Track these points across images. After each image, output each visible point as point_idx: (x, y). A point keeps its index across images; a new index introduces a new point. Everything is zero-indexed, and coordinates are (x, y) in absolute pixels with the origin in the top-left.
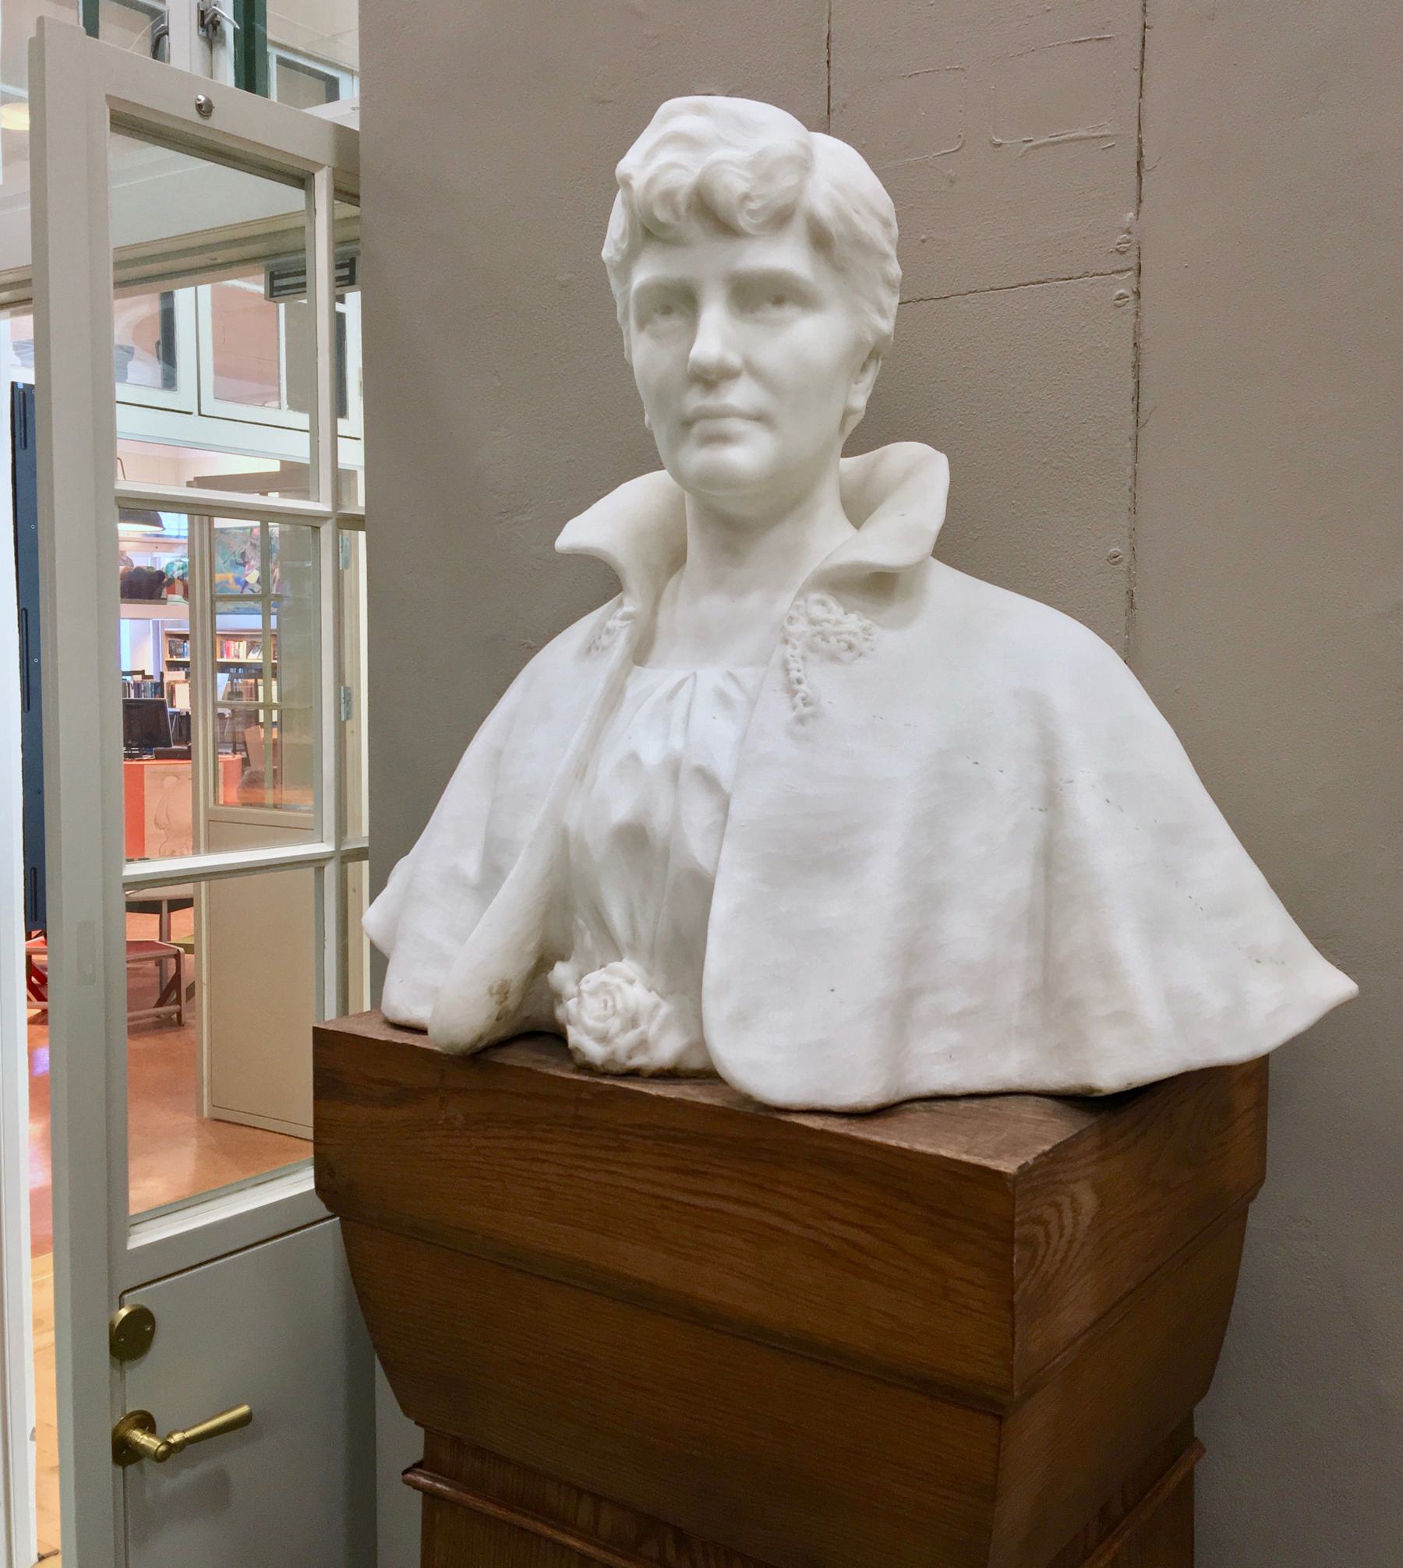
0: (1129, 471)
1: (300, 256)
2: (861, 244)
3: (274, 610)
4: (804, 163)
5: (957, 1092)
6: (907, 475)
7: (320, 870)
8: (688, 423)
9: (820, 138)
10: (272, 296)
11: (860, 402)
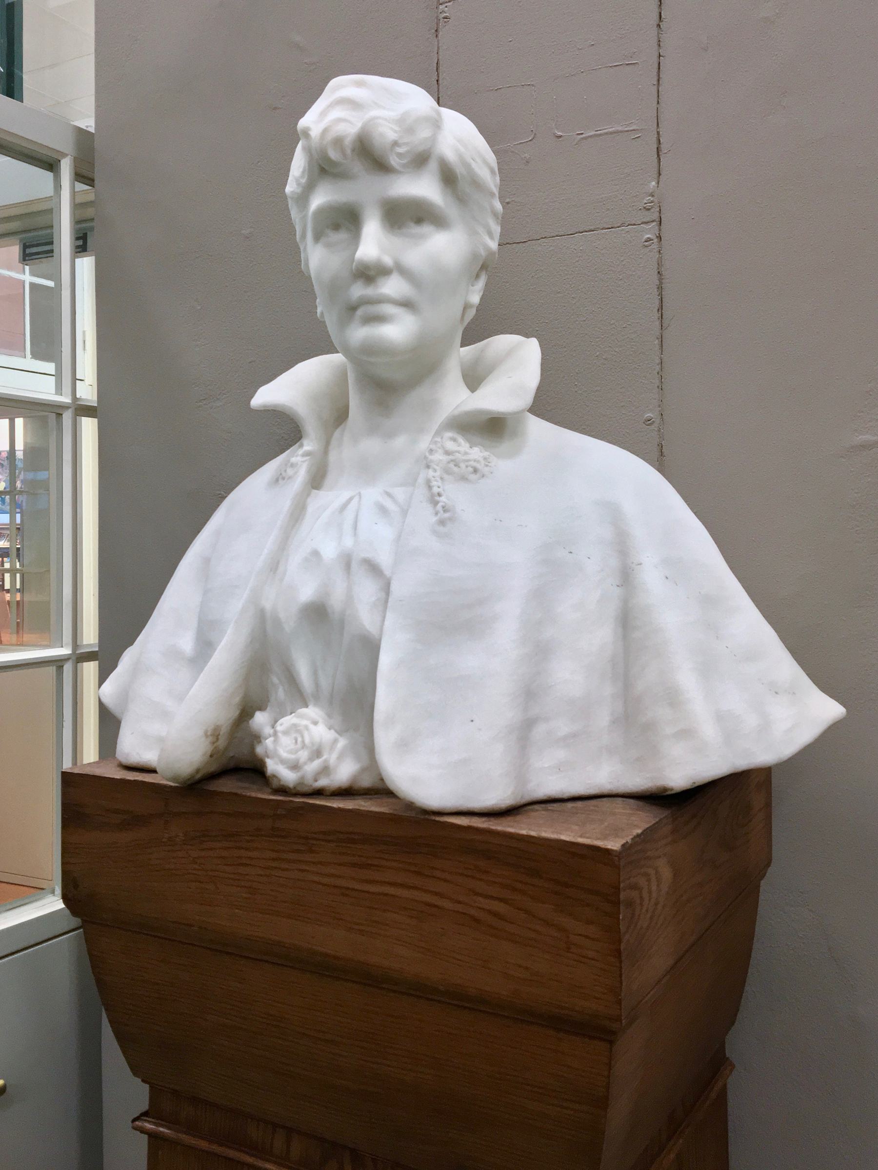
0: (658, 361)
1: (49, 231)
2: (476, 183)
3: (18, 510)
4: (437, 124)
6: (510, 353)
7: (60, 668)
8: (353, 308)
9: (446, 112)
10: (24, 260)
11: (475, 299)
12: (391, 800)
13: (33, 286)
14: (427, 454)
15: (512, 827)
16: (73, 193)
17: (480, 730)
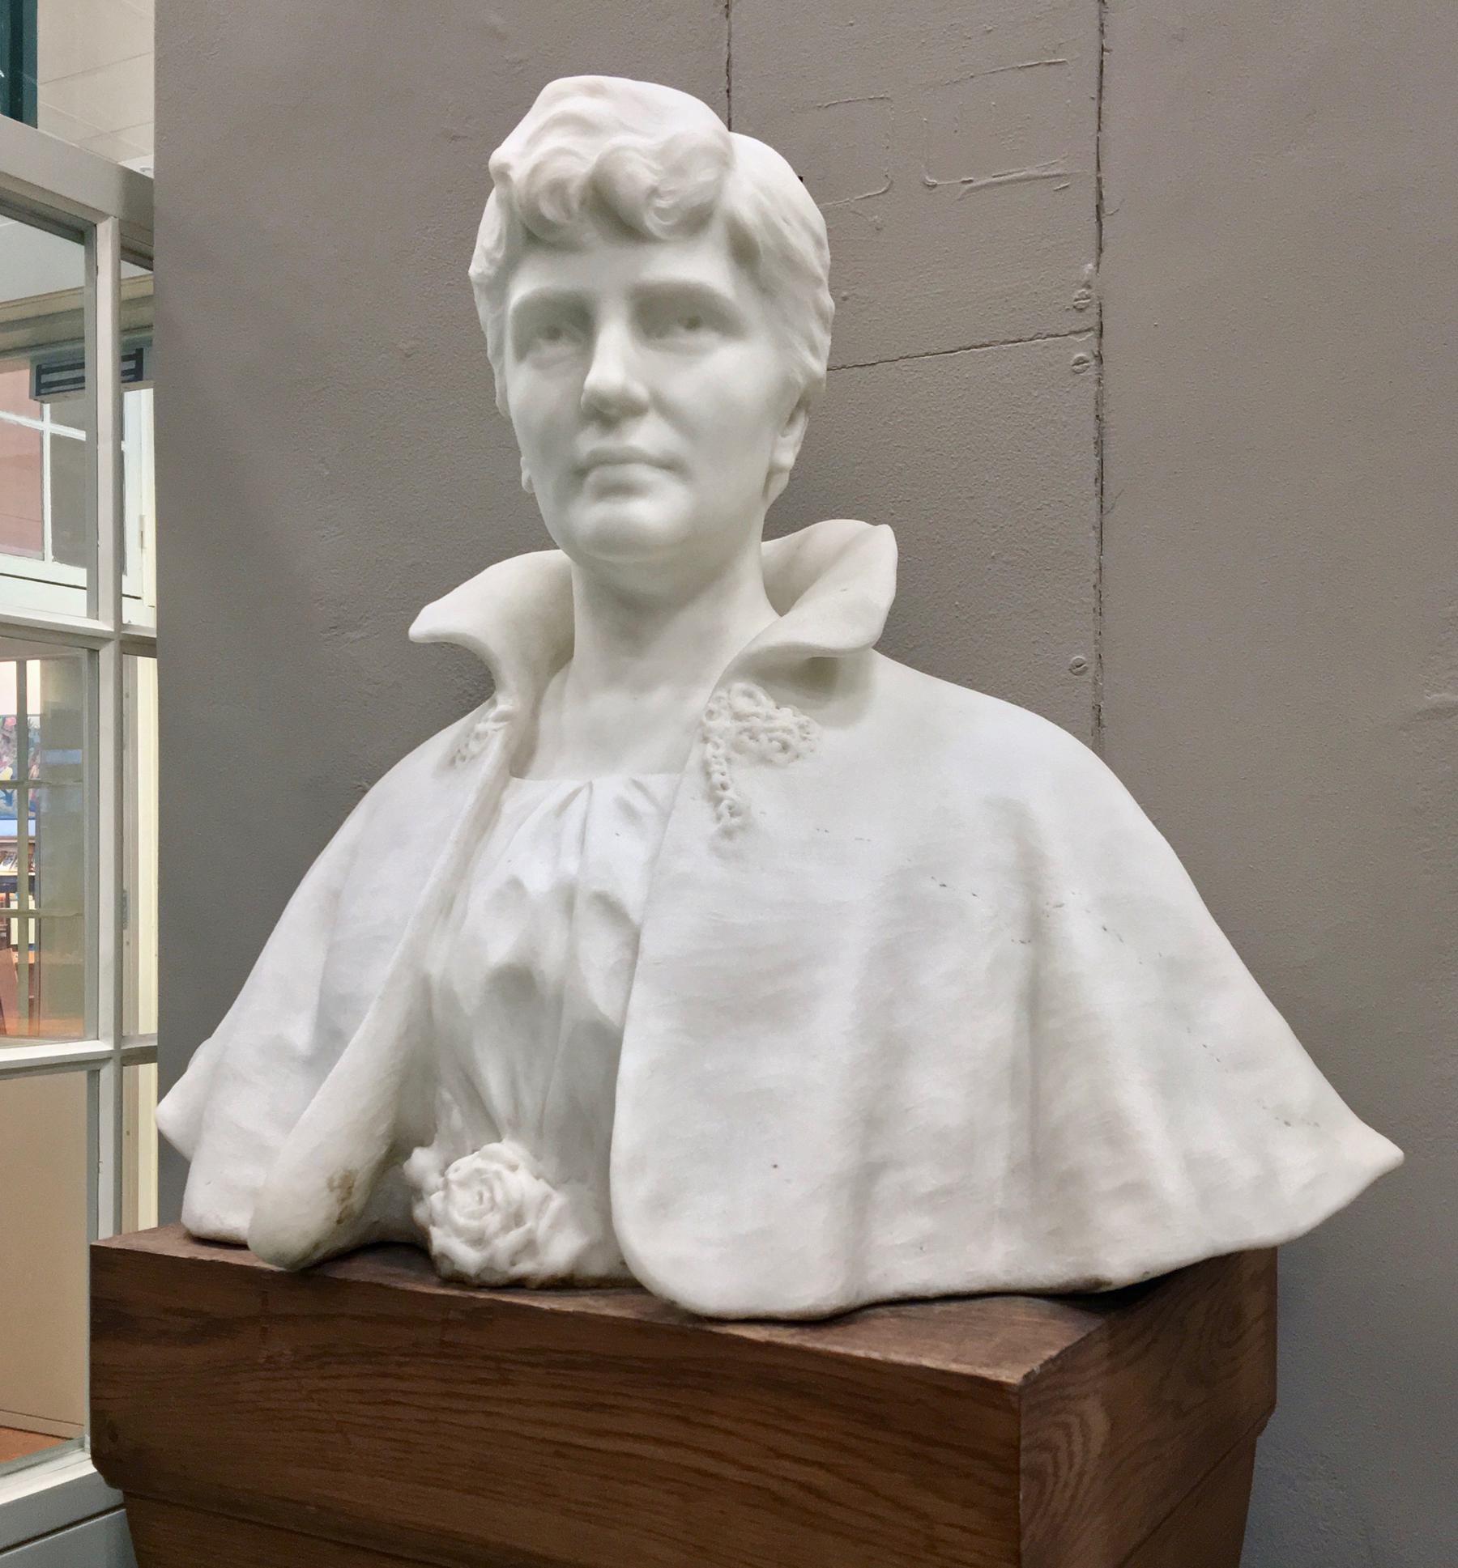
1: (78, 346)
2: (790, 261)
3: (32, 814)
4: (724, 160)
5: (930, 1293)
6: (843, 550)
7: (94, 1075)
8: (580, 472)
10: (38, 393)
11: (787, 458)
12: (638, 1298)
13: (56, 439)
14: (704, 719)
15: (841, 1344)
16: (118, 282)
17: (788, 1181)
